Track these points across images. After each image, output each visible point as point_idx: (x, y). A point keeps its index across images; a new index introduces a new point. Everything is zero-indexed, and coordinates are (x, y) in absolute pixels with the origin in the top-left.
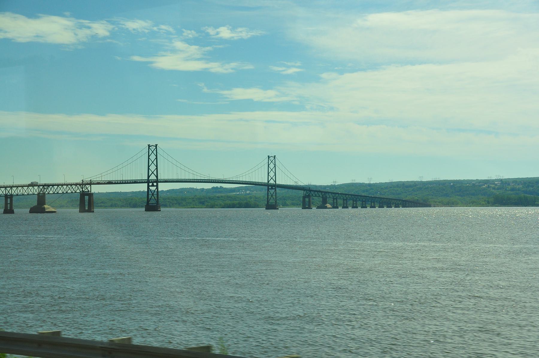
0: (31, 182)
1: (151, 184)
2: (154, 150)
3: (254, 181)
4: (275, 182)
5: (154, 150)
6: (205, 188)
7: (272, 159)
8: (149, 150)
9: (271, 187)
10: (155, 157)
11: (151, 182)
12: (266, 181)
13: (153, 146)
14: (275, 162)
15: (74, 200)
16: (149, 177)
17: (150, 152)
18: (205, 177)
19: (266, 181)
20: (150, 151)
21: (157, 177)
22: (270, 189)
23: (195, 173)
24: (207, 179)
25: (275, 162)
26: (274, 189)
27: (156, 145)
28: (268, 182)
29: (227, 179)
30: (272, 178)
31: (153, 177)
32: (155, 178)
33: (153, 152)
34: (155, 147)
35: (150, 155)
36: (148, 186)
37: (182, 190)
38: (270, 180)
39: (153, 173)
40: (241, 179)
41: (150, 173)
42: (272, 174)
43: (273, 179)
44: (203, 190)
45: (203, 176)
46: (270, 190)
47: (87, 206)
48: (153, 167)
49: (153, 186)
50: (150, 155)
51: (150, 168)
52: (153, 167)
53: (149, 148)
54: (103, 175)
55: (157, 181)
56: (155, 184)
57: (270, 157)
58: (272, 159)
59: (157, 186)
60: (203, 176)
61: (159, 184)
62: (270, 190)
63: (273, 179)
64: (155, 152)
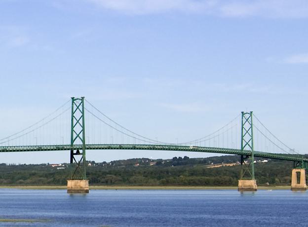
0: (185, 157)
1: (75, 152)
2: (80, 104)
3: (221, 147)
4: (252, 148)
5: (80, 104)
6: (151, 158)
7: (78, 102)
8: (73, 104)
9: (243, 156)
10: (81, 114)
11: (75, 149)
12: (240, 148)
13: (78, 99)
14: (251, 120)
15: (141, 172)
16: (72, 141)
17: (75, 108)
18: (152, 141)
19: (240, 148)
20: (74, 105)
21: (83, 141)
22: (75, 154)
23: (137, 137)
24: (152, 144)
25: (251, 120)
26: (81, 154)
27: (83, 98)
28: (242, 148)
29: (182, 145)
30: (247, 143)
31: (78, 142)
32: (82, 143)
33: (78, 108)
34: (81, 101)
35: (74, 111)
36: (72, 154)
37: (131, 162)
38: (75, 140)
39: (78, 136)
40: (202, 145)
41: (75, 135)
42: (247, 138)
43: (249, 145)
44: (159, 162)
45: (143, 139)
46: (74, 156)
47: (247, 181)
48: (78, 129)
49: (78, 153)
50: (74, 111)
51: (82, 129)
52: (78, 129)
53: (73, 102)
54: (10, 138)
55: (85, 147)
56: (81, 151)
57: (75, 100)
58: (246, 117)
59: (84, 154)
60: (143, 139)
61: (87, 151)
62: (74, 156)
63: (249, 145)
64: (81, 107)
